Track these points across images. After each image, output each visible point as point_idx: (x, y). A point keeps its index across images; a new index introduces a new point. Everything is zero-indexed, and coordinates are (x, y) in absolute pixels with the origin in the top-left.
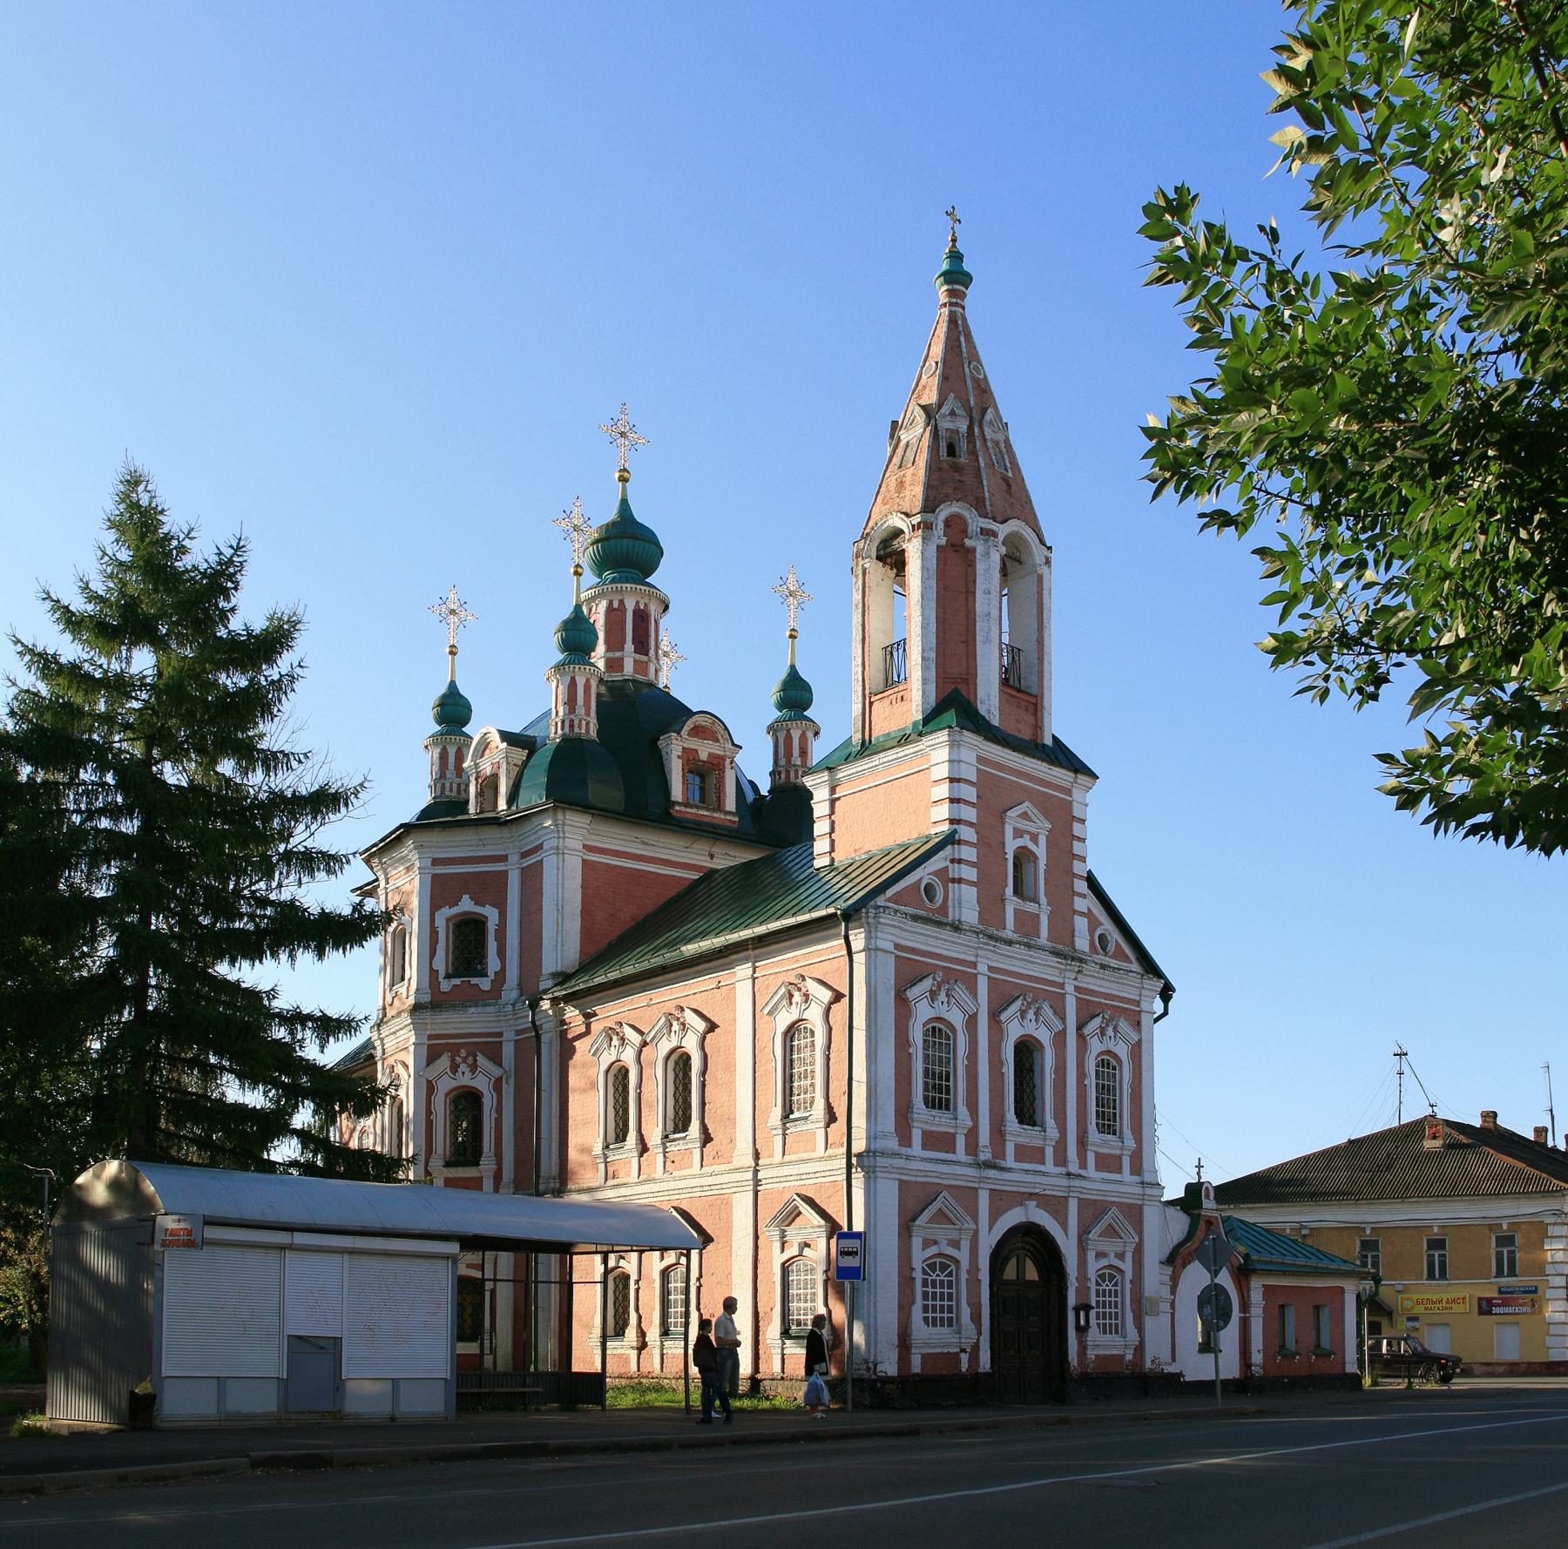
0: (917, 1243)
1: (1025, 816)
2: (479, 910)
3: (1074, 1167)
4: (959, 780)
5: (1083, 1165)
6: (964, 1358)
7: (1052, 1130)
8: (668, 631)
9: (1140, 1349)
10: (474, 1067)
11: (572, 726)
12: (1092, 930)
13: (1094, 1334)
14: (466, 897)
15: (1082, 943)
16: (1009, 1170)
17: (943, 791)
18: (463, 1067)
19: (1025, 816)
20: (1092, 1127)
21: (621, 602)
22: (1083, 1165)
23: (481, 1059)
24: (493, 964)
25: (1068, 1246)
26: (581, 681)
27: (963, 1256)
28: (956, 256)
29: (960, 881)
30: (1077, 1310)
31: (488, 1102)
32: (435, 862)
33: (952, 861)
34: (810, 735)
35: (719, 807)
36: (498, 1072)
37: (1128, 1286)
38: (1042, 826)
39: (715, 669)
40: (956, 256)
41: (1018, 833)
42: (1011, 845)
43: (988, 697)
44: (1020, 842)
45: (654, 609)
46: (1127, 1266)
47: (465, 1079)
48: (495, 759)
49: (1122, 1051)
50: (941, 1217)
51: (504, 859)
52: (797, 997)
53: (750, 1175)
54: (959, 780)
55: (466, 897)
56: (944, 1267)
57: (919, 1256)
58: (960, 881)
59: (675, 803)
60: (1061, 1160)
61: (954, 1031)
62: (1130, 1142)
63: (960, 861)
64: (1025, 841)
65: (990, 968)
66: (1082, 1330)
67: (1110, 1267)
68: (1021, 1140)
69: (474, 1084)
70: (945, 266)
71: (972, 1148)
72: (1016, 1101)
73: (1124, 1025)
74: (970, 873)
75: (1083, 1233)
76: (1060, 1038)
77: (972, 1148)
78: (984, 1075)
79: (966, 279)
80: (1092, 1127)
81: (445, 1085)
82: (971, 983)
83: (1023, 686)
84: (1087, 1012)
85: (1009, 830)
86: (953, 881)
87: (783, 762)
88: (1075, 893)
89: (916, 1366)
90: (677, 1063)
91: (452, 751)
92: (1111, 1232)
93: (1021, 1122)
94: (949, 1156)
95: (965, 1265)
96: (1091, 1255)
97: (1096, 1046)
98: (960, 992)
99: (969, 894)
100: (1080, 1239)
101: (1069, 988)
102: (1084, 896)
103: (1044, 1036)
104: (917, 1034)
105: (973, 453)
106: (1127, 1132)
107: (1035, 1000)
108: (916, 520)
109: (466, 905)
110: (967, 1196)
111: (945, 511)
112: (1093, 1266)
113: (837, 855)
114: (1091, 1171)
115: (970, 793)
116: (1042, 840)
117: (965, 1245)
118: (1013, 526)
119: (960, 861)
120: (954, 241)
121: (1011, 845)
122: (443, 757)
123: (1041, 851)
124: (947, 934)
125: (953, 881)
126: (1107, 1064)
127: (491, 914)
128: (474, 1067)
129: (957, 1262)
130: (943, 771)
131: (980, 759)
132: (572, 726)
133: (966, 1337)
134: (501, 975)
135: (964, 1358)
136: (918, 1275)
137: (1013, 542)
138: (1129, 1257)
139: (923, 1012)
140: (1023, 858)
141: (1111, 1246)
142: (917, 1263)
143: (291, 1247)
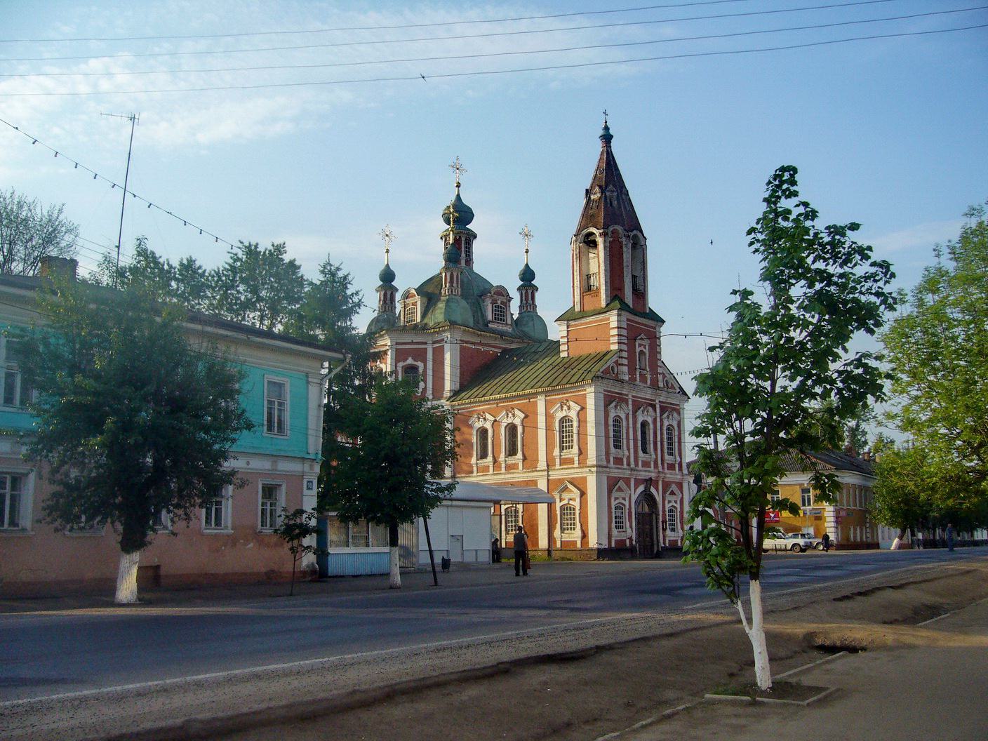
1: (642, 339)
2: (415, 363)
3: (660, 469)
4: (621, 328)
5: (663, 468)
6: (628, 541)
7: (654, 456)
11: (452, 291)
12: (664, 378)
13: (668, 532)
14: (410, 358)
15: (661, 385)
16: (641, 471)
17: (615, 332)
20: (666, 454)
21: (460, 237)
25: (659, 498)
26: (455, 274)
27: (627, 503)
28: (607, 128)
29: (622, 365)
30: (663, 522)
32: (397, 344)
33: (620, 357)
37: (678, 513)
38: (646, 342)
39: (494, 262)
40: (607, 128)
43: (629, 297)
44: (640, 349)
46: (678, 506)
48: (712, 435)
49: (675, 424)
51: (426, 343)
52: (565, 407)
53: (546, 473)
54: (621, 328)
55: (410, 358)
57: (614, 503)
58: (622, 365)
59: (490, 322)
61: (622, 420)
62: (678, 459)
63: (622, 357)
64: (642, 348)
65: (633, 396)
66: (664, 530)
67: (673, 506)
68: (644, 459)
71: (629, 464)
72: (288, 342)
73: (675, 414)
74: (625, 362)
75: (664, 493)
76: (655, 421)
77: (629, 464)
78: (630, 434)
80: (666, 454)
82: (626, 401)
83: (640, 294)
84: (663, 410)
86: (620, 364)
87: (524, 302)
88: (658, 366)
89: (613, 545)
90: (510, 429)
91: (389, 293)
92: (672, 493)
93: (644, 453)
94: (649, 469)
95: (627, 507)
96: (666, 502)
97: (666, 423)
98: (624, 406)
99: (625, 369)
100: (663, 496)
101: (657, 402)
102: (661, 367)
103: (650, 420)
104: (611, 422)
106: (677, 454)
107: (646, 407)
108: (601, 231)
109: (410, 361)
110: (627, 481)
111: (611, 229)
112: (667, 506)
113: (570, 351)
114: (666, 471)
115: (624, 332)
117: (627, 499)
118: (635, 232)
119: (622, 357)
120: (606, 122)
121: (638, 350)
122: (385, 295)
123: (647, 351)
125: (620, 364)
126: (670, 428)
127: (420, 365)
129: (624, 505)
130: (615, 324)
131: (628, 320)
132: (452, 291)
133: (630, 532)
135: (628, 541)
136: (667, 513)
137: (635, 236)
138: (679, 502)
139: (612, 414)
141: (672, 498)
142: (667, 510)
143: (451, 506)
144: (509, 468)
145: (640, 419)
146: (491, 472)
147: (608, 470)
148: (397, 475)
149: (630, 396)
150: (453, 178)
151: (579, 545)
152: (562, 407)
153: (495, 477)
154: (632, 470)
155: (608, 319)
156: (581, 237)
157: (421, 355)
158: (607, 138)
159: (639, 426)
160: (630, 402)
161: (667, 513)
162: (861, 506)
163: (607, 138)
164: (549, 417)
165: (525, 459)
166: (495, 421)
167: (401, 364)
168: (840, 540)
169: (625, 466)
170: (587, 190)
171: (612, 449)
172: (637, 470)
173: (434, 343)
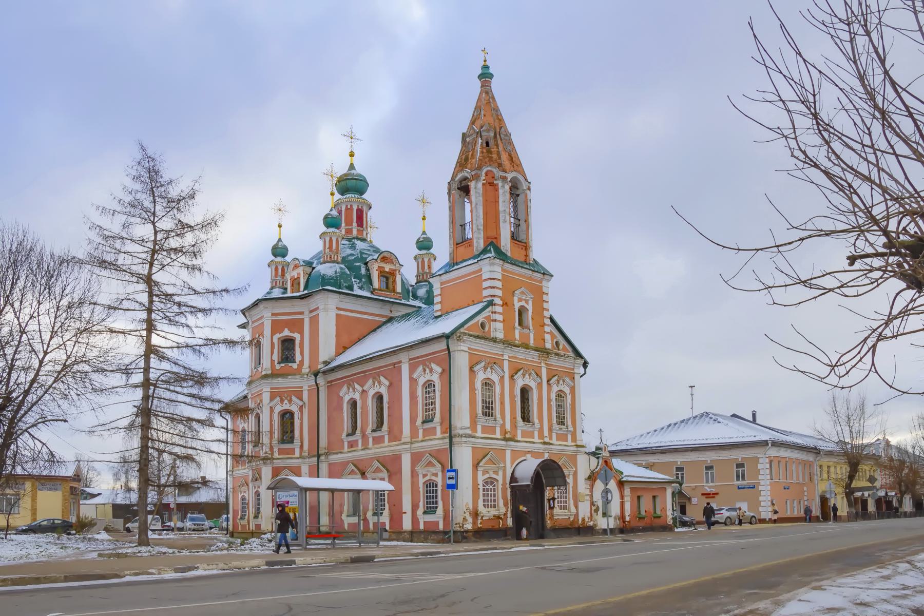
0: (480, 473)
1: (522, 293)
8: (372, 216)
9: (577, 515)
10: (290, 401)
13: (557, 511)
18: (286, 401)
19: (522, 293)
22: (551, 438)
23: (294, 398)
24: (298, 357)
27: (500, 478)
28: (485, 67)
31: (297, 416)
34: (432, 260)
35: (394, 291)
36: (301, 403)
40: (485, 67)
41: (520, 300)
42: (517, 305)
45: (365, 209)
47: (286, 406)
50: (491, 461)
51: (302, 313)
56: (492, 483)
58: (495, 321)
60: (541, 435)
64: (523, 303)
66: (551, 508)
69: (380, 390)
70: (480, 72)
79: (491, 76)
81: (278, 409)
85: (516, 299)
93: (524, 421)
99: (500, 326)
104: (478, 385)
105: (497, 146)
106: (569, 424)
109: (286, 333)
116: (530, 303)
117: (501, 473)
123: (530, 307)
124: (491, 344)
127: (297, 336)
128: (290, 401)
129: (497, 481)
134: (302, 362)
136: (481, 487)
139: (481, 376)
140: (522, 311)
144: (378, 440)
145: (520, 382)
146: (360, 447)
147: (473, 440)
148: (241, 456)
149: (506, 357)
150: (346, 146)
151: (441, 527)
152: (425, 370)
153: (350, 455)
154: (545, 443)
155: (481, 270)
156: (455, 185)
157: (297, 326)
158: (485, 76)
159: (518, 392)
160: (506, 364)
161: (481, 487)
162: (798, 478)
163: (485, 76)
164: (413, 381)
165: (389, 432)
166: (363, 391)
167: (278, 336)
168: (627, 519)
169: (536, 440)
170: (464, 134)
171: (556, 426)
172: (474, 437)
173: (311, 312)
